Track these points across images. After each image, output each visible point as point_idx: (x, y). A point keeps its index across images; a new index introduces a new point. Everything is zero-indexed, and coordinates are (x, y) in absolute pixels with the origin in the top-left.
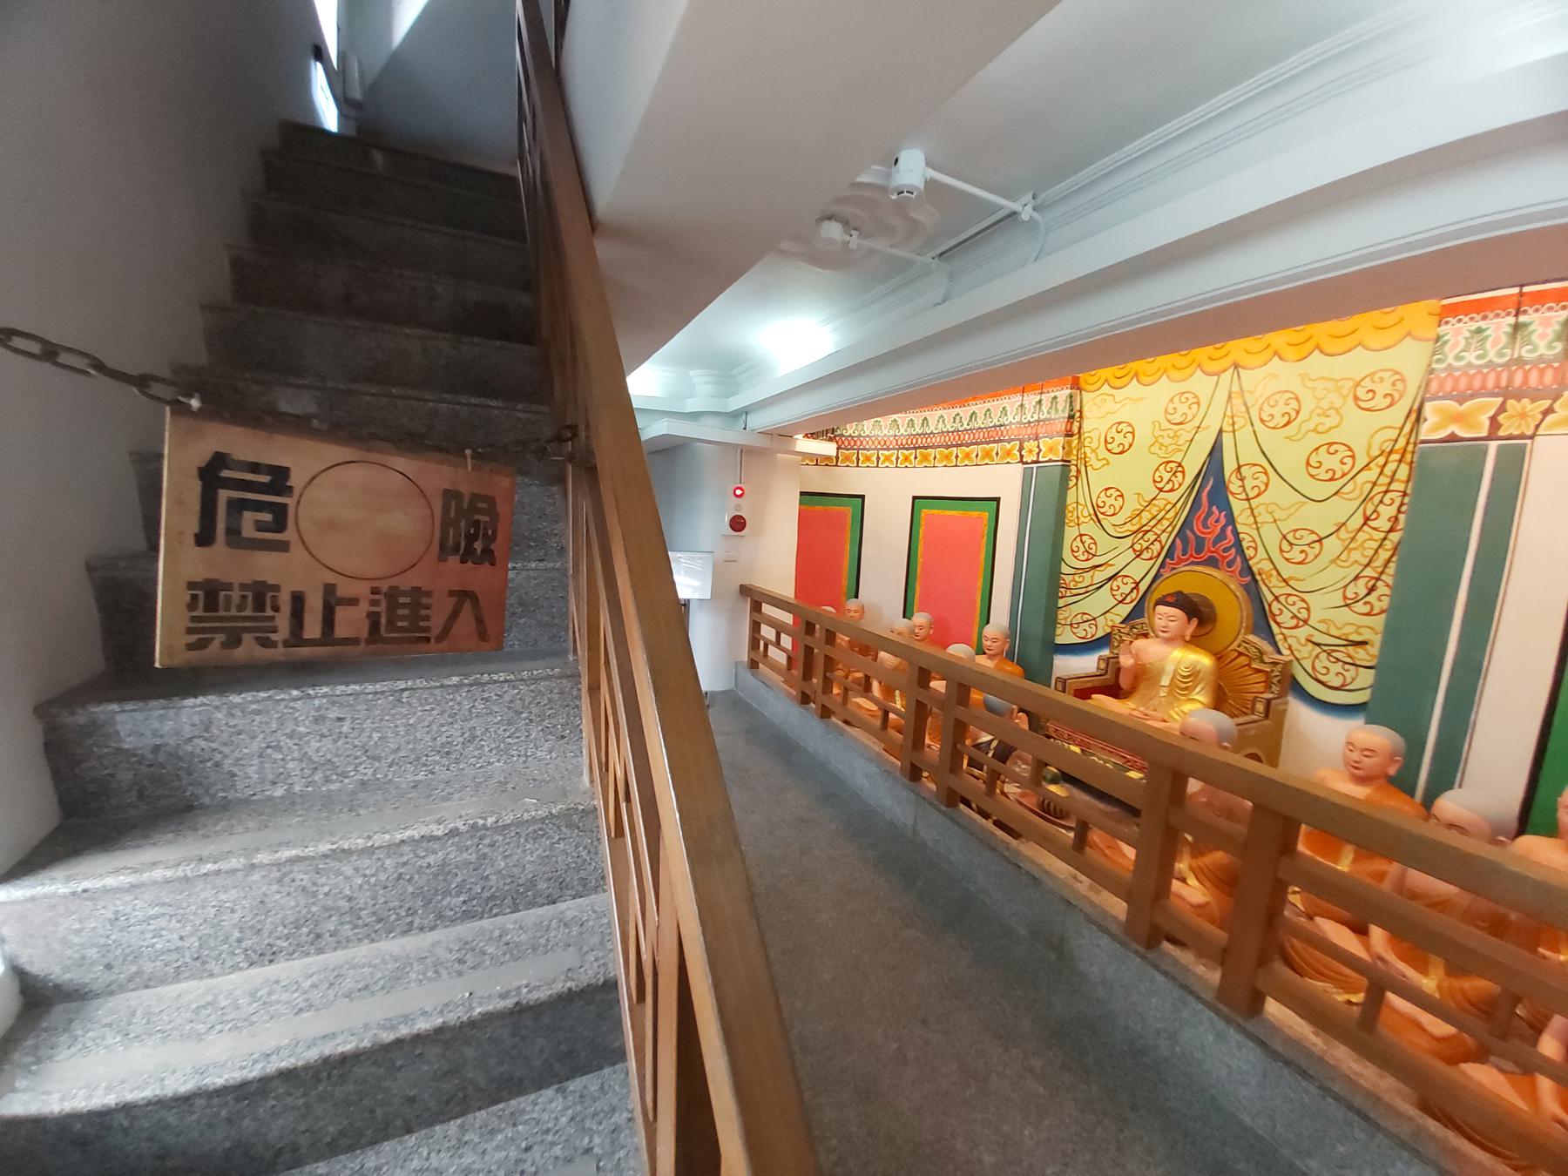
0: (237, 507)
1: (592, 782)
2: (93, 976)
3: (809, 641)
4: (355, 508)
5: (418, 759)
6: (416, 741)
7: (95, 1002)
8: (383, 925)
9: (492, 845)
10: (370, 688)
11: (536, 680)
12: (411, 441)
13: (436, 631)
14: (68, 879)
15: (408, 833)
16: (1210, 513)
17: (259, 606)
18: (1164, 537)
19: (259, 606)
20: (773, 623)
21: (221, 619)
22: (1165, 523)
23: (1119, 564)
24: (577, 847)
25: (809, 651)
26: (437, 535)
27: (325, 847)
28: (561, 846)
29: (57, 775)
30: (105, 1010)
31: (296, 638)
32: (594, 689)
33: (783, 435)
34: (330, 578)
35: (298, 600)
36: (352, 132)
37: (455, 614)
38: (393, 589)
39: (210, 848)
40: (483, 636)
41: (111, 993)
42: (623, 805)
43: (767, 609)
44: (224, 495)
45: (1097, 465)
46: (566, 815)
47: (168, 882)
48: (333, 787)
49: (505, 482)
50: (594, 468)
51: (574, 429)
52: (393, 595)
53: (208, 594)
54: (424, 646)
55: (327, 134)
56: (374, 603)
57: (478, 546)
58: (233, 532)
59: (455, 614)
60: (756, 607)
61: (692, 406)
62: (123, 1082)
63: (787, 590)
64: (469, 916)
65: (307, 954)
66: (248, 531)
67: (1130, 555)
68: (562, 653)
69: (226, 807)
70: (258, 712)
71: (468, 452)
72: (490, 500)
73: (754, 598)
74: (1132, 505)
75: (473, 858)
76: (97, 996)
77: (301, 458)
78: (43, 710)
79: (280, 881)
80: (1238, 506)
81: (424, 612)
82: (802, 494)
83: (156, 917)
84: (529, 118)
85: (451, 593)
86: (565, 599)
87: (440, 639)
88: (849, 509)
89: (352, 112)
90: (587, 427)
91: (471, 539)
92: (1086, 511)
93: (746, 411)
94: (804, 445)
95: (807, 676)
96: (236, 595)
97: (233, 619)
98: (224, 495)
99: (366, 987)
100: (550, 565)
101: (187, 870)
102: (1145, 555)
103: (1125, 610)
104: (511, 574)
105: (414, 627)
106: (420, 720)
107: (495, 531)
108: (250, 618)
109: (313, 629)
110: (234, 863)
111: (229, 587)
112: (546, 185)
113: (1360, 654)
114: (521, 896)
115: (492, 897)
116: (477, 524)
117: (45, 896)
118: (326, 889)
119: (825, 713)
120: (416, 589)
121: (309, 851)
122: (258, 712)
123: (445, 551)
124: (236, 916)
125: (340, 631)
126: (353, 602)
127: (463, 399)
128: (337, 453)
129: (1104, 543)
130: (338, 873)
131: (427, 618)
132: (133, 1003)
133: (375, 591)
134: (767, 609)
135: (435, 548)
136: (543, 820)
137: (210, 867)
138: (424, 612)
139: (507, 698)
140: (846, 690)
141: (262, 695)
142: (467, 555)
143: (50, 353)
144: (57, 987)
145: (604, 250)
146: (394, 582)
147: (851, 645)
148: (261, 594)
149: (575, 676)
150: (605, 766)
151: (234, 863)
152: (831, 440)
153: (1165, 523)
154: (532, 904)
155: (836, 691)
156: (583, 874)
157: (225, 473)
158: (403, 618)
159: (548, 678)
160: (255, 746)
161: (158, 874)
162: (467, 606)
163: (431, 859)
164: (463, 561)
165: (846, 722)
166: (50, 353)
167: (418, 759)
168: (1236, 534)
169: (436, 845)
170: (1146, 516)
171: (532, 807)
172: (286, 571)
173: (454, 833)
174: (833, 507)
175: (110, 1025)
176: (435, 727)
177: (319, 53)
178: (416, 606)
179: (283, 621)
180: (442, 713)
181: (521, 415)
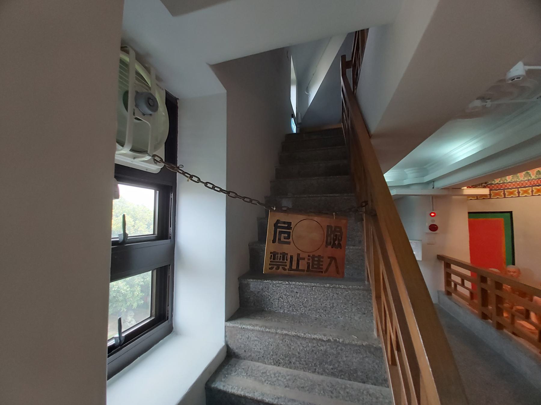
0: (281, 233)
1: (378, 335)
2: (241, 352)
3: (484, 286)
4: (307, 232)
5: (317, 310)
6: (316, 304)
7: (241, 361)
8: (307, 367)
9: (341, 350)
10: (305, 284)
11: (354, 289)
12: (319, 211)
13: (324, 269)
14: (241, 324)
15: (315, 336)
17: (283, 259)
19: (283, 259)
20: (458, 274)
21: (277, 262)
24: (373, 362)
25: (484, 292)
26: (325, 239)
27: (294, 333)
28: (367, 359)
29: (240, 297)
30: (246, 364)
31: (291, 269)
32: (378, 298)
33: (456, 188)
34: (299, 252)
35: (291, 257)
36: (299, 132)
37: (330, 264)
38: (313, 255)
39: (268, 324)
40: (338, 272)
41: (245, 359)
42: (396, 352)
43: (453, 267)
44: (278, 230)
46: (366, 346)
47: (259, 331)
48: (294, 313)
49: (344, 221)
50: (375, 215)
51: (366, 203)
52: (314, 256)
53: (274, 255)
54: (321, 274)
55: (534, 312)
56: (309, 260)
57: (336, 242)
58: (279, 239)
59: (330, 264)
60: (447, 265)
61: (406, 182)
62: (246, 389)
63: (466, 259)
64: (333, 374)
65: (287, 367)
66: (282, 239)
68: (363, 280)
69: (270, 312)
70: (279, 287)
71: (334, 214)
72: (340, 228)
73: (447, 263)
75: (335, 353)
76: (242, 359)
77: (294, 219)
78: (239, 279)
79: (282, 340)
81: (321, 263)
82: (469, 213)
83: (256, 340)
84: (346, 111)
85: (329, 257)
86: (363, 260)
87: (325, 272)
88: (501, 219)
89: (298, 126)
90: (372, 201)
91: (335, 240)
93: (433, 181)
94: (467, 191)
95: (485, 302)
96: (279, 255)
97: (277, 262)
98: (278, 230)
99: (303, 387)
100: (357, 248)
101: (262, 329)
104: (347, 252)
105: (321, 267)
106: (318, 297)
107: (341, 238)
108: (281, 262)
109: (294, 267)
110: (273, 331)
111: (278, 253)
112: (353, 128)
114: (351, 374)
115: (341, 371)
116: (336, 236)
117: (236, 327)
118: (293, 347)
119: (499, 327)
120: (319, 256)
121: (290, 333)
122: (279, 287)
123: (327, 244)
124: (272, 347)
125: (300, 268)
126: (304, 259)
127: (328, 195)
128: (301, 217)
130: (296, 343)
131: (322, 265)
132: (249, 364)
133: (309, 256)
134: (453, 267)
135: (325, 243)
136: (359, 346)
137: (268, 330)
138: (321, 263)
139: (344, 294)
140: (513, 316)
141: (280, 282)
142: (334, 246)
143: (251, 201)
144: (234, 353)
145: (373, 142)
146: (314, 253)
147: (513, 290)
148: (284, 255)
149: (369, 290)
150: (385, 332)
151: (273, 331)
152: (485, 187)
154: (355, 380)
155: (505, 315)
156: (376, 375)
157: (279, 225)
158: (316, 265)
159: (358, 289)
160: (278, 296)
161: (257, 328)
162: (333, 262)
163: (322, 348)
164: (332, 248)
165: (514, 333)
166: (251, 201)
167: (317, 310)
169: (323, 344)
171: (354, 339)
172: (290, 250)
173: (329, 341)
174: (491, 218)
175: (243, 369)
176: (322, 300)
177: (293, 116)
178: (319, 261)
179: (288, 264)
180: (324, 296)
181: (346, 198)
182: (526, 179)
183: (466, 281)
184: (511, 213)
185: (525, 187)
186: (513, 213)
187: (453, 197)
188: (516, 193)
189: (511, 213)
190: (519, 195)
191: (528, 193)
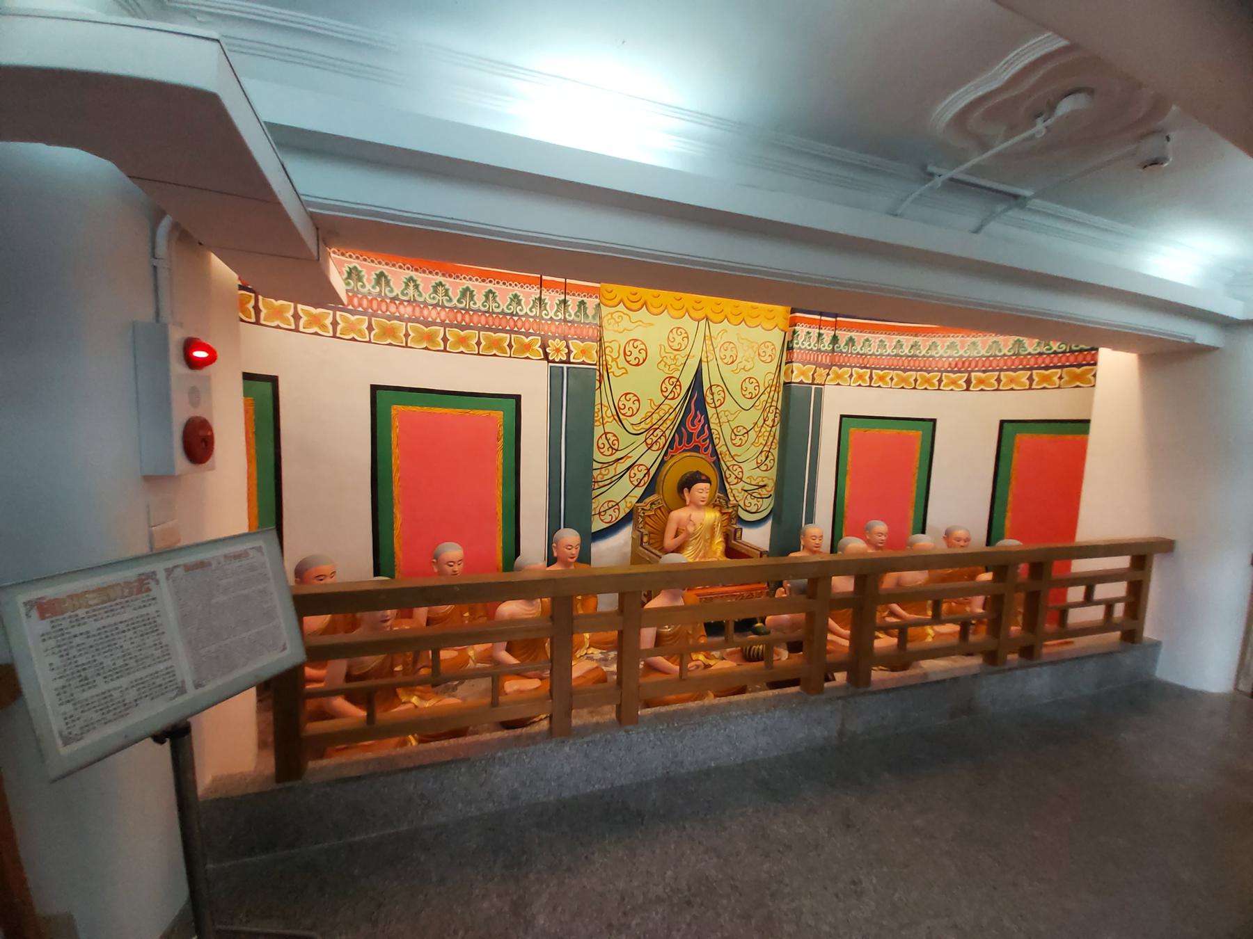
16: (696, 416)
18: (667, 433)
22: (669, 422)
23: (635, 455)
45: (618, 372)
67: (644, 447)
74: (646, 408)
80: (711, 411)
92: (609, 413)
102: (655, 447)
103: (639, 492)
113: (764, 492)
129: (625, 439)
153: (669, 422)
168: (710, 429)
170: (656, 417)
188: (935, 381)
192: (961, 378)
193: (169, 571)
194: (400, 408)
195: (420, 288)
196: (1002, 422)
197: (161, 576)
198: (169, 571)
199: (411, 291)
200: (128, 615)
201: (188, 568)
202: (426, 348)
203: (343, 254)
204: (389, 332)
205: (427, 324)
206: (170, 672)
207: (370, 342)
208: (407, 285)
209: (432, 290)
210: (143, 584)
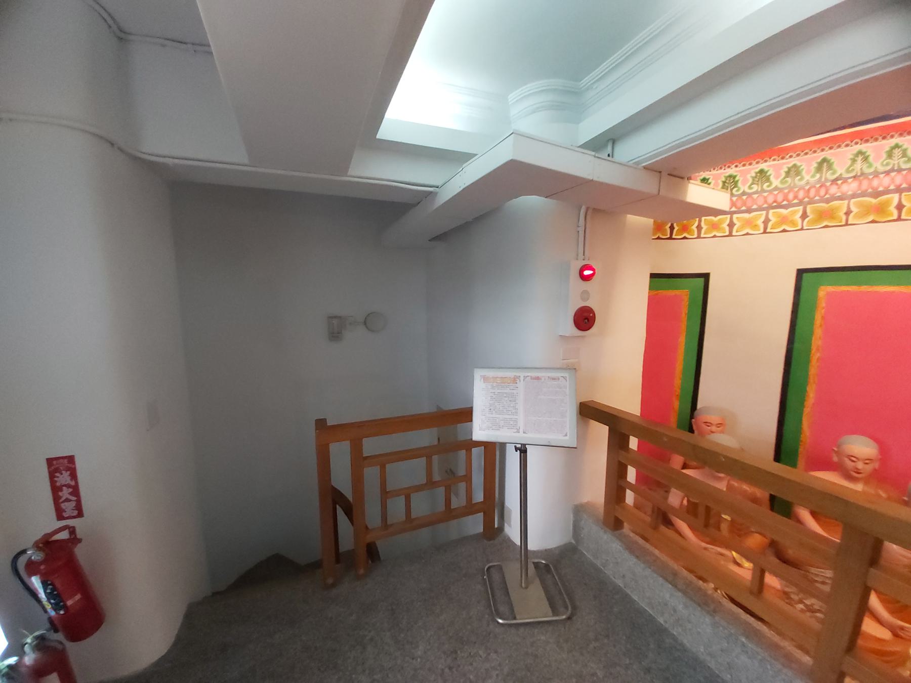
82: (653, 276)
125: (402, 500)
182: (755, 188)
183: (480, 516)
184: (706, 277)
185: (749, 211)
186: (77, 460)
187: (629, 216)
188: (725, 226)
189: (706, 277)
190: (731, 232)
191: (756, 227)
192: (795, 212)
193: (525, 377)
194: (830, 289)
195: (871, 159)
196: (801, 273)
197: (522, 378)
198: (525, 377)
199: (859, 165)
200: (508, 391)
201: (532, 378)
202: (873, 222)
203: (783, 158)
204: (823, 215)
205: (876, 194)
206: (516, 421)
207: (802, 229)
208: (854, 161)
209: (885, 156)
210: (515, 380)
